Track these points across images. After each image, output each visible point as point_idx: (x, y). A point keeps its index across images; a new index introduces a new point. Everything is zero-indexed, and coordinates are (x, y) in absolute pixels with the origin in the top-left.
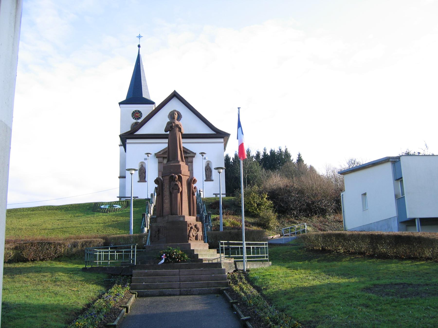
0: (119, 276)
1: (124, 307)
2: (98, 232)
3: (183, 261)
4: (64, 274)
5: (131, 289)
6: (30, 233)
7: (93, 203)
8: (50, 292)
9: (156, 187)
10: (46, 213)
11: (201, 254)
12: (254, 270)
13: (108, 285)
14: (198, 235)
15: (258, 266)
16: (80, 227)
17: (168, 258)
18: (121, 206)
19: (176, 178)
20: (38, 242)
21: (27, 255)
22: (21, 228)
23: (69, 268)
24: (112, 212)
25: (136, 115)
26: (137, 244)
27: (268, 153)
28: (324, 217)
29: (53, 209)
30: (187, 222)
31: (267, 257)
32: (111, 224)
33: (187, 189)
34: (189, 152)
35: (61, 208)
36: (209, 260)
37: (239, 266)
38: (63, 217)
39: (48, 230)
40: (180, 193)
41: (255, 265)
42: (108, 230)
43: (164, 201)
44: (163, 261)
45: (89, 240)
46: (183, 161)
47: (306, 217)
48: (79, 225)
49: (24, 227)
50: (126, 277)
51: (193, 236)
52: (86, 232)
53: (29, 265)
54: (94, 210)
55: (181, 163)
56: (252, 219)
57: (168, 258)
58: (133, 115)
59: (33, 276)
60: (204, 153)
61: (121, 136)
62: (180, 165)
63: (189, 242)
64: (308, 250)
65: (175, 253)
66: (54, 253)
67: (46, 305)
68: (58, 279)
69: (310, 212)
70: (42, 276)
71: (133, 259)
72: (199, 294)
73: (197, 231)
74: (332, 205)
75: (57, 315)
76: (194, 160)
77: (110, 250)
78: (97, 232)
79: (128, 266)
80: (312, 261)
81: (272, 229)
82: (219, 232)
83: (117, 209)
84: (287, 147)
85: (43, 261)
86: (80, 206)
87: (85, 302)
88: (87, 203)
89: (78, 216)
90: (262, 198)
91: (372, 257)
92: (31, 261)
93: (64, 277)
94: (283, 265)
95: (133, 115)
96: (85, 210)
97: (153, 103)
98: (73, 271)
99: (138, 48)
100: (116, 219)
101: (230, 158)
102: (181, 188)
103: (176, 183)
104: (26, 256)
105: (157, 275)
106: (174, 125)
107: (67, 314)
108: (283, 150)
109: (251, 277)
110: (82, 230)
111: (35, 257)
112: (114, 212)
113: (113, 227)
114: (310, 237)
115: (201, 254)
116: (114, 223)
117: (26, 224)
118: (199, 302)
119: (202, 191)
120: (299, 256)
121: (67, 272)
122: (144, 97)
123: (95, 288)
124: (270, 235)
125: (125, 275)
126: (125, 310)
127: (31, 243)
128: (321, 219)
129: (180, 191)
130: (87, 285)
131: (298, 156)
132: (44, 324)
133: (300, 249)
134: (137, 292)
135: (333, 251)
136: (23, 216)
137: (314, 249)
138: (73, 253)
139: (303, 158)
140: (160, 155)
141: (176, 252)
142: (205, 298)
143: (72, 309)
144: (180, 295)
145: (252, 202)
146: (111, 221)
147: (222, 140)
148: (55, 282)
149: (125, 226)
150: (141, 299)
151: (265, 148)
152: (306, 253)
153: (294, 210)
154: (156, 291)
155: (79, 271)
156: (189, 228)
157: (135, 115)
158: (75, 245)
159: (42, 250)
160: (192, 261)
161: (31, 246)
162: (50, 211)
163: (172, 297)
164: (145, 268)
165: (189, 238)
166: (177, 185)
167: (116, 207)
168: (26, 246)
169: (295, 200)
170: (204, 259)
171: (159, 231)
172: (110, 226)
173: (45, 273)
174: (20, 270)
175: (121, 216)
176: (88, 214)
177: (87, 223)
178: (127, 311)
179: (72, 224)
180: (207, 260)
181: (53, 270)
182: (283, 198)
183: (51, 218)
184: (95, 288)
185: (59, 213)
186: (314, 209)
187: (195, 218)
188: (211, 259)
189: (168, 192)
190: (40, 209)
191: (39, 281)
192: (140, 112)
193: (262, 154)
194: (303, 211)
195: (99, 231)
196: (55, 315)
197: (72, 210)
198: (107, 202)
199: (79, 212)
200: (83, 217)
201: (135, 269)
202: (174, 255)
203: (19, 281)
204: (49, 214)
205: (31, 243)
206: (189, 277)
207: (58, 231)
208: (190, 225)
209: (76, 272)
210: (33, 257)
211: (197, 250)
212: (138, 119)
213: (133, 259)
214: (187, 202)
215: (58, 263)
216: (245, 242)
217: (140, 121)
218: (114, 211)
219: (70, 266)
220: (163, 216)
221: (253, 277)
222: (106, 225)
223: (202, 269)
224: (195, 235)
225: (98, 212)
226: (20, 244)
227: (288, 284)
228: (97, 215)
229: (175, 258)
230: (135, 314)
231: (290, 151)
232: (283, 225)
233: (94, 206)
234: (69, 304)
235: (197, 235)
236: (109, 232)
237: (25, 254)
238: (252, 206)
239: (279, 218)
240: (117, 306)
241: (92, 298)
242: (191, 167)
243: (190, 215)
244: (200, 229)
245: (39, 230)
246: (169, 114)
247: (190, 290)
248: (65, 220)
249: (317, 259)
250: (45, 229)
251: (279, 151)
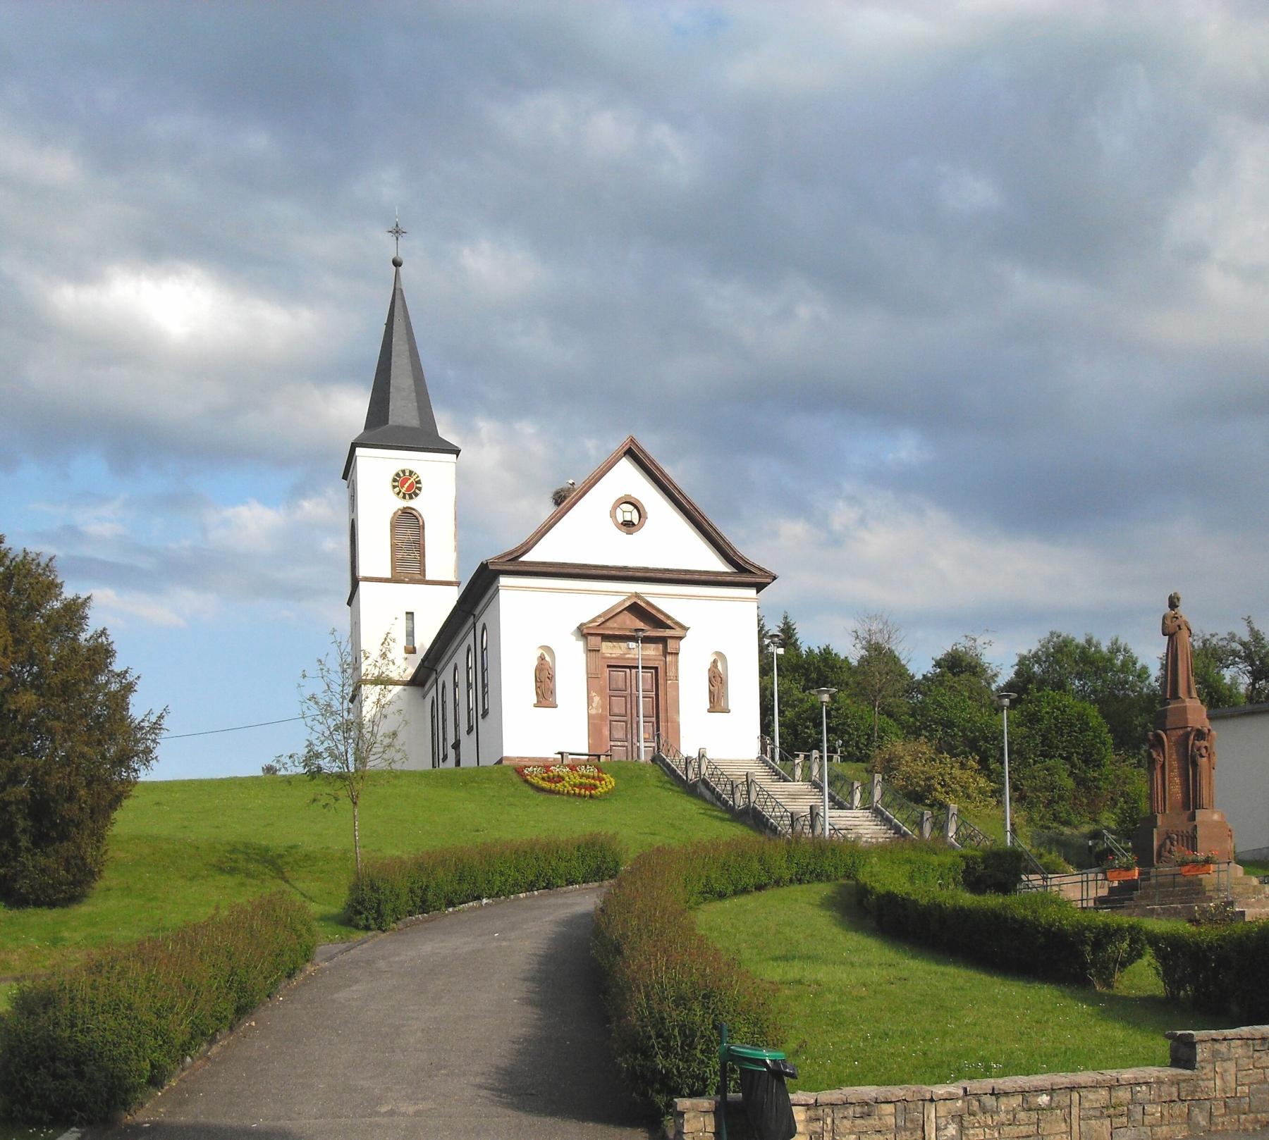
34: (672, 625)
95: (396, 484)
140: (592, 628)
227: (152, 934)
242: (673, 670)
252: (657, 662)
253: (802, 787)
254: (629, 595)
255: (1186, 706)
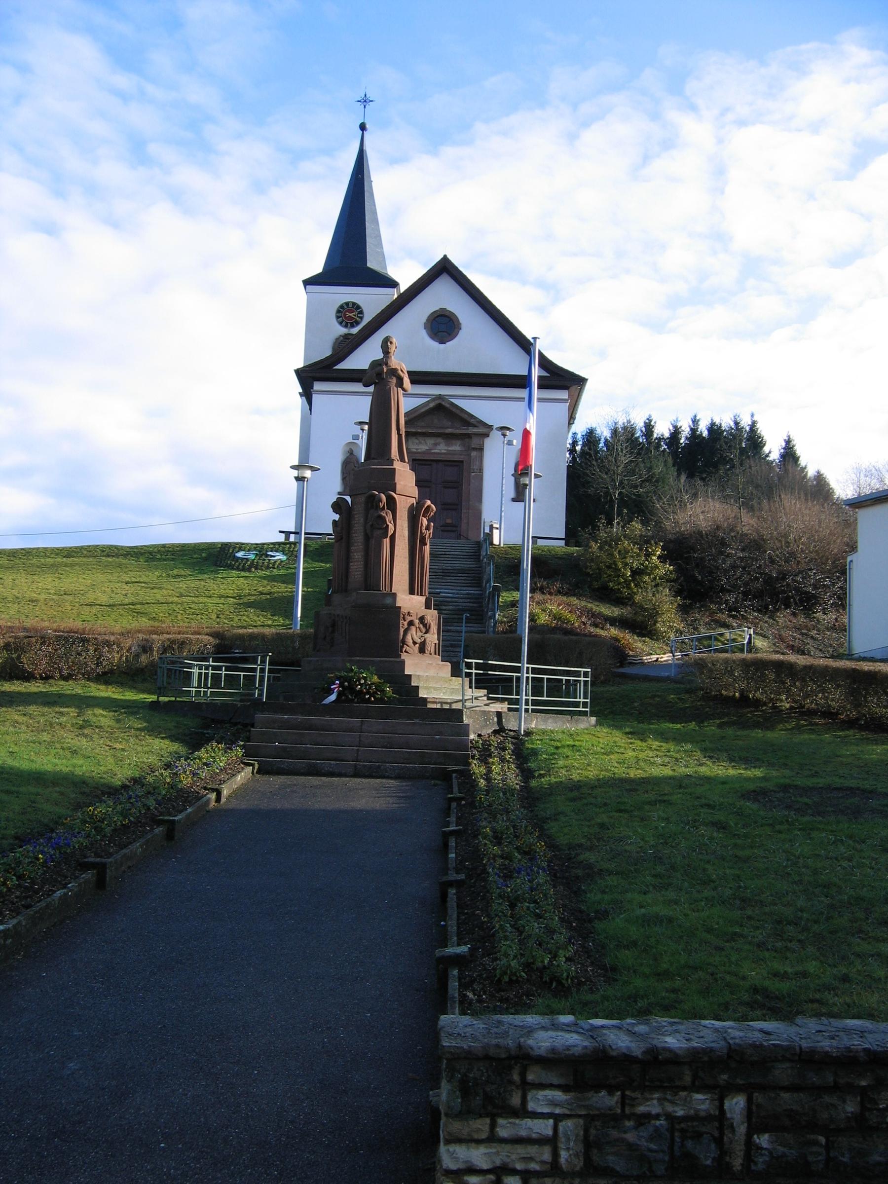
0: (227, 725)
1: (213, 790)
2: (218, 620)
3: (381, 701)
4: (105, 713)
5: (247, 754)
6: (55, 613)
7: (219, 543)
8: (63, 748)
9: (334, 521)
10: (100, 564)
11: (427, 688)
12: (544, 732)
13: (195, 742)
14: (427, 641)
15: (559, 724)
16: (177, 603)
17: (346, 692)
18: (286, 555)
19: (381, 500)
20: (57, 637)
21: (32, 664)
22: (34, 599)
23: (126, 700)
24: (262, 570)
25: (348, 314)
26: (270, 654)
27: (703, 430)
28: (808, 616)
29: (117, 556)
30: (400, 608)
31: (585, 705)
32: (255, 600)
33: (407, 529)
34: (475, 423)
35: (137, 554)
36: (442, 703)
37: (508, 721)
38: (140, 577)
39: (98, 607)
40: (388, 539)
41: (550, 721)
42: (244, 615)
43: (351, 554)
44: (333, 697)
45: (179, 637)
46: (402, 459)
47: (759, 611)
48: (176, 599)
49: (43, 597)
50: (241, 727)
51: (415, 643)
52: (190, 616)
53: (34, 687)
54: (219, 563)
55: (398, 465)
56: (615, 609)
57: (346, 692)
58: (340, 315)
59: (35, 713)
60: (508, 429)
61: (301, 374)
62: (395, 469)
63: (402, 658)
64: (707, 697)
65: (362, 681)
66: (94, 664)
67: (46, 773)
68: (89, 722)
69: (772, 598)
70: (56, 713)
71: (259, 688)
72: (396, 778)
73: (426, 633)
74: (834, 585)
75: (62, 794)
76: (488, 443)
77: (211, 664)
78: (218, 617)
79: (249, 703)
80: (706, 724)
81: (664, 637)
82: (516, 635)
83: (275, 562)
84: (755, 418)
85: (67, 681)
86: (185, 550)
87: (132, 773)
88: (202, 543)
89: (178, 576)
90: (648, 555)
91: (851, 724)
92: (42, 678)
93: (103, 717)
94: (618, 727)
95: (340, 315)
96: (195, 560)
97: (393, 284)
98: (128, 707)
99: (361, 132)
100: (269, 587)
101: (600, 440)
102: (391, 526)
103: (382, 513)
104: (28, 666)
105: (310, 728)
106: (385, 371)
107: (83, 793)
108: (746, 422)
109: (528, 749)
110: (181, 612)
111: (50, 671)
112: (268, 571)
113: (257, 608)
114: (713, 665)
115: (427, 688)
116: (264, 597)
117: (47, 589)
118: (389, 793)
119: (497, 528)
120: (681, 709)
121: (114, 709)
122: (372, 267)
123: (164, 747)
124: (651, 654)
125: (239, 722)
126: (213, 796)
127: (42, 638)
128: (802, 619)
129: (390, 533)
130: (149, 740)
131: (784, 444)
132: (30, 806)
133: (688, 691)
134: (256, 763)
135: (765, 704)
136: (43, 568)
137: (722, 695)
138: (141, 666)
139: (799, 450)
141: (365, 678)
142: (406, 786)
143: (97, 784)
144: (356, 775)
145: (620, 565)
146: (255, 592)
147: (564, 394)
148: (81, 727)
149: (284, 606)
150: (266, 778)
151: (695, 416)
152: (699, 703)
153: (729, 591)
154: (301, 763)
155: (142, 708)
156: (406, 623)
157: (345, 315)
158: (146, 648)
159: (66, 655)
160: (401, 702)
161: (41, 644)
162: (110, 559)
163: (335, 779)
164: (284, 709)
165: (402, 647)
166: (383, 519)
167: (274, 556)
168: (29, 644)
169: (734, 567)
170: (431, 700)
171: (334, 625)
172: (250, 605)
173: (64, 708)
174: (11, 698)
175: (284, 582)
176: (202, 572)
177: (195, 594)
178: (218, 799)
179: (159, 595)
180: (439, 702)
181: (83, 703)
182: (702, 559)
183: (110, 577)
184: (164, 747)
185: (132, 564)
186: (784, 592)
187: (422, 599)
188: (449, 701)
189: (362, 534)
190: (85, 552)
191: (48, 724)
192: (358, 307)
193: (686, 431)
194: (755, 597)
195: (221, 616)
196: (59, 792)
197: (165, 560)
198: (252, 544)
199: (181, 566)
200: (188, 578)
201: (262, 712)
202: (360, 684)
203: (5, 721)
204: (105, 566)
205: (42, 638)
206: (383, 738)
207: (123, 612)
208: (408, 617)
209: (135, 710)
210: (44, 669)
211: (419, 676)
212: (353, 326)
213: (259, 688)
214: (407, 561)
215: (102, 687)
216: (526, 665)
217: (355, 330)
218: (268, 568)
219: (130, 695)
220: (346, 591)
221: (532, 749)
222: (241, 601)
223: (417, 721)
224: (419, 641)
225: (228, 567)
226: (16, 638)
228: (225, 575)
229: (361, 691)
230: (234, 806)
231: (763, 429)
232: (696, 629)
233: (219, 552)
234: (94, 774)
235: (425, 640)
236: (247, 620)
237: (26, 662)
238: (619, 576)
239: (684, 610)
240: (198, 786)
241: (151, 767)
242: (477, 463)
243: (412, 592)
244: (434, 628)
245: (77, 605)
246: (428, 320)
247: (379, 767)
248: (143, 585)
249: (720, 718)
250: (90, 605)
251: (733, 429)
252: (462, 457)
253: (472, 566)
254: (433, 397)
255: (395, 469)
